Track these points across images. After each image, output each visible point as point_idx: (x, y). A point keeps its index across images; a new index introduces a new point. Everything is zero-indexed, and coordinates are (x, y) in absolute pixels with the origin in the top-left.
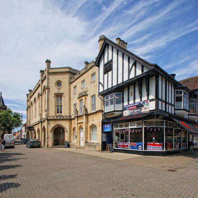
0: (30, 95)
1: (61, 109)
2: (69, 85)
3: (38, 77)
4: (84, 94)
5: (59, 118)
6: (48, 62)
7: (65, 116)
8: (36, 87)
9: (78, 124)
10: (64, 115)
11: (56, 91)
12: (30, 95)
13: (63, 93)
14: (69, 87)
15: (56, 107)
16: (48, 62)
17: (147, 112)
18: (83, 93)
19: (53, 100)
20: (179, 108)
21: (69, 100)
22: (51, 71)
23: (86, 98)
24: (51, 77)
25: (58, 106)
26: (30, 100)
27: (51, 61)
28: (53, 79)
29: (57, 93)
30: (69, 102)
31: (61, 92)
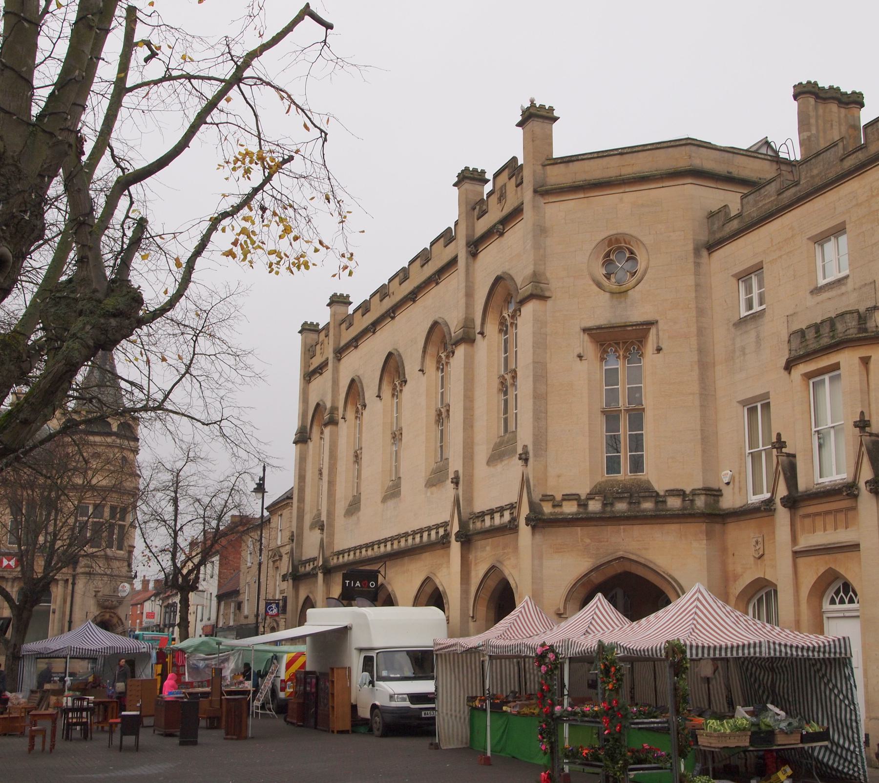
0: (338, 336)
1: (637, 443)
2: (697, 265)
3: (445, 211)
4: (853, 332)
5: (621, 507)
6: (537, 118)
7: (567, 497)
8: (403, 275)
9: (801, 561)
10: (660, 486)
11: (601, 311)
12: (338, 336)
13: (650, 324)
14: (697, 273)
15: (601, 422)
16: (537, 118)
17: (595, 523)
18: (840, 327)
19: (580, 378)
20: (740, 693)
21: (696, 373)
22: (557, 176)
23: (865, 361)
24: (558, 211)
25: (611, 417)
26: (336, 371)
27: (556, 114)
28: (576, 228)
29: (599, 328)
30: (695, 388)
31: (637, 314)
